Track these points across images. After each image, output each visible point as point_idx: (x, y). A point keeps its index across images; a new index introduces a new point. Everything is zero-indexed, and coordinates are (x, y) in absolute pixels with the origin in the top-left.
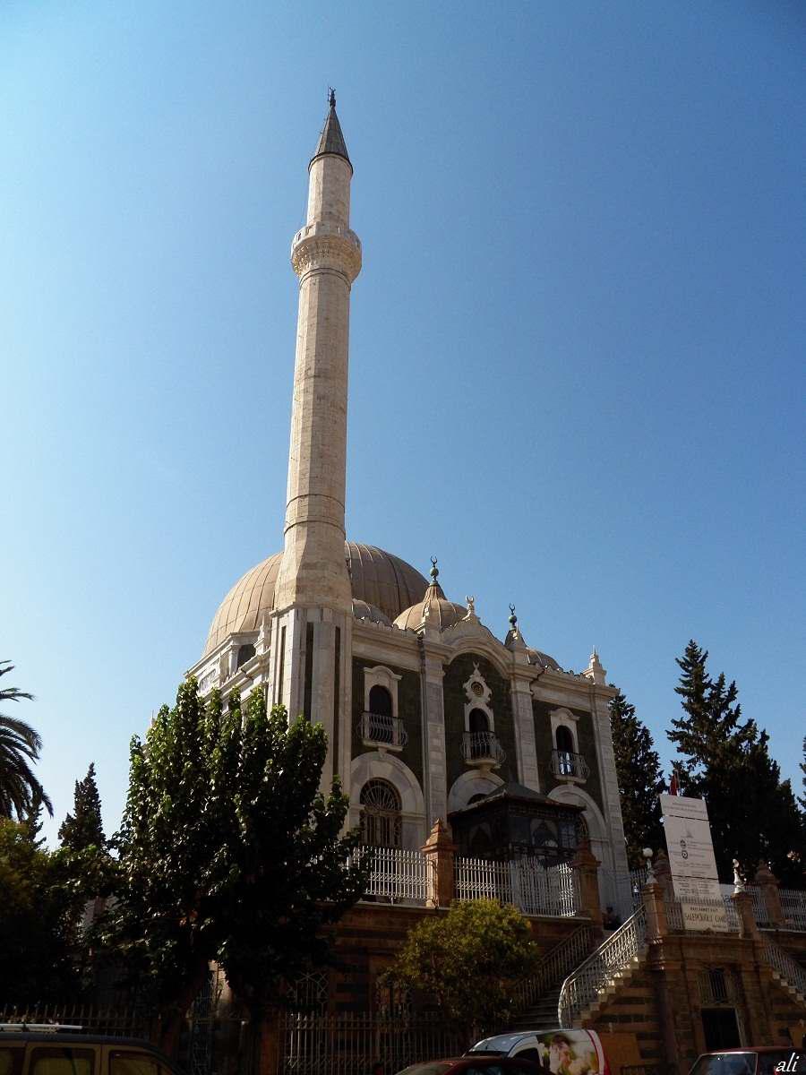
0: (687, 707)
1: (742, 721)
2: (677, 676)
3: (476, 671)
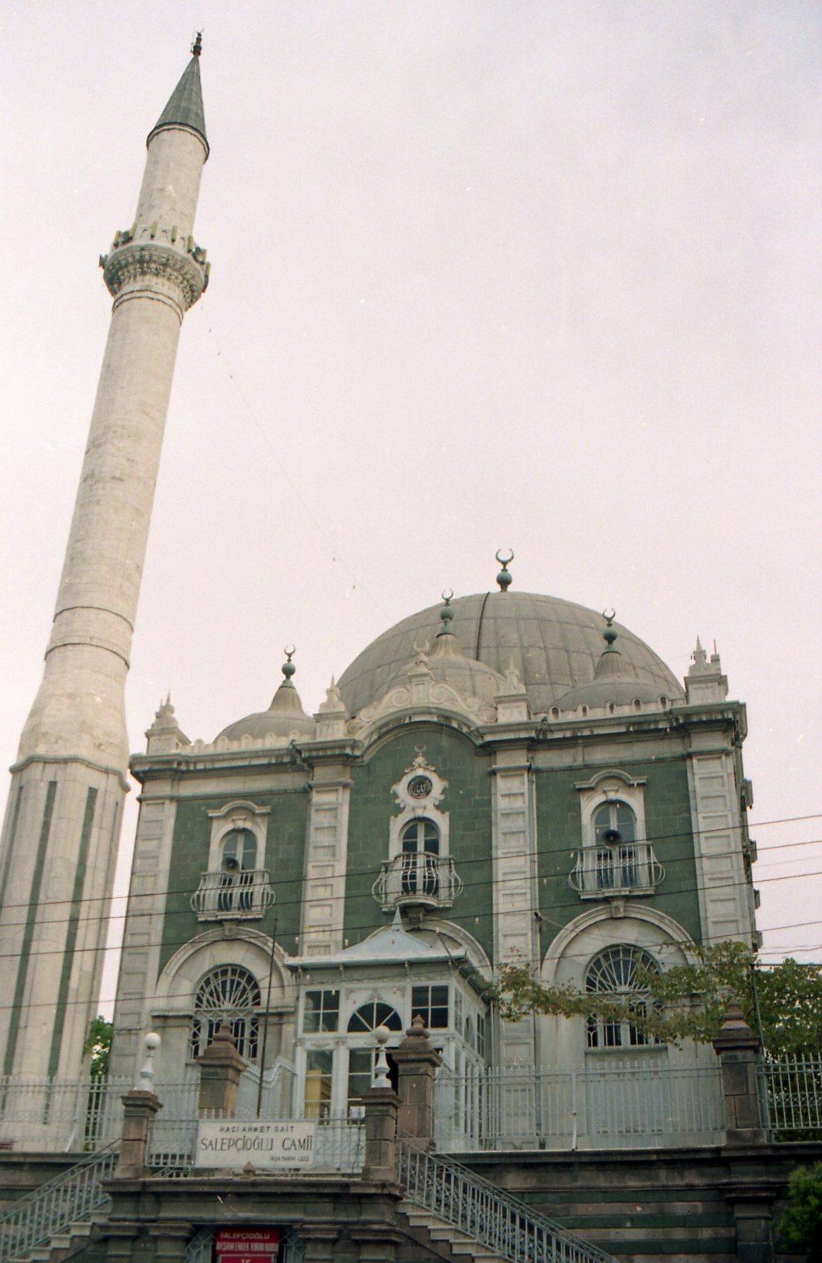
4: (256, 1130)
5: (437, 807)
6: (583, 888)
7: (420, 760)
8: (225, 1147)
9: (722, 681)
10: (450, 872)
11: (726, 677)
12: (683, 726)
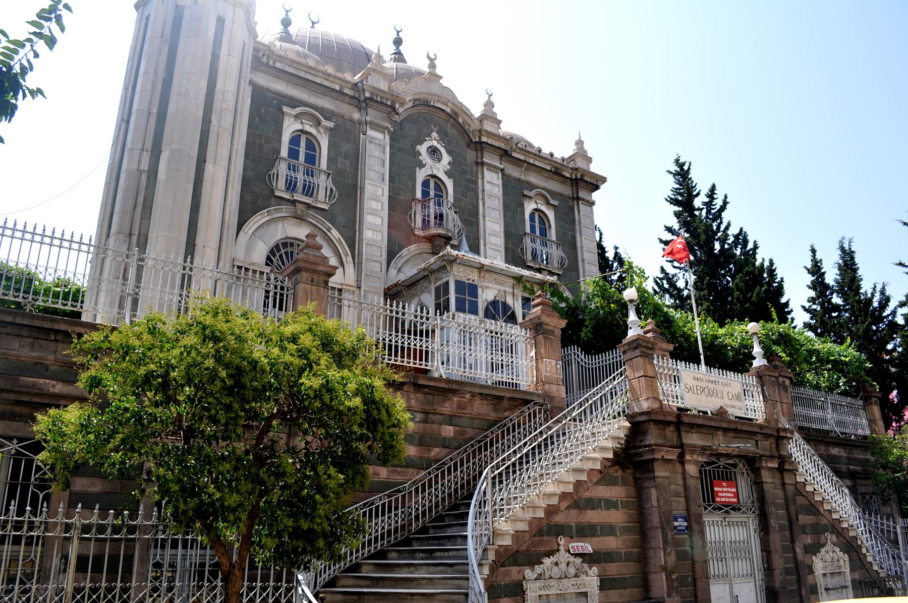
0: (677, 215)
1: (734, 231)
2: (670, 184)
3: (434, 134)
5: (446, 173)
12: (576, 179)
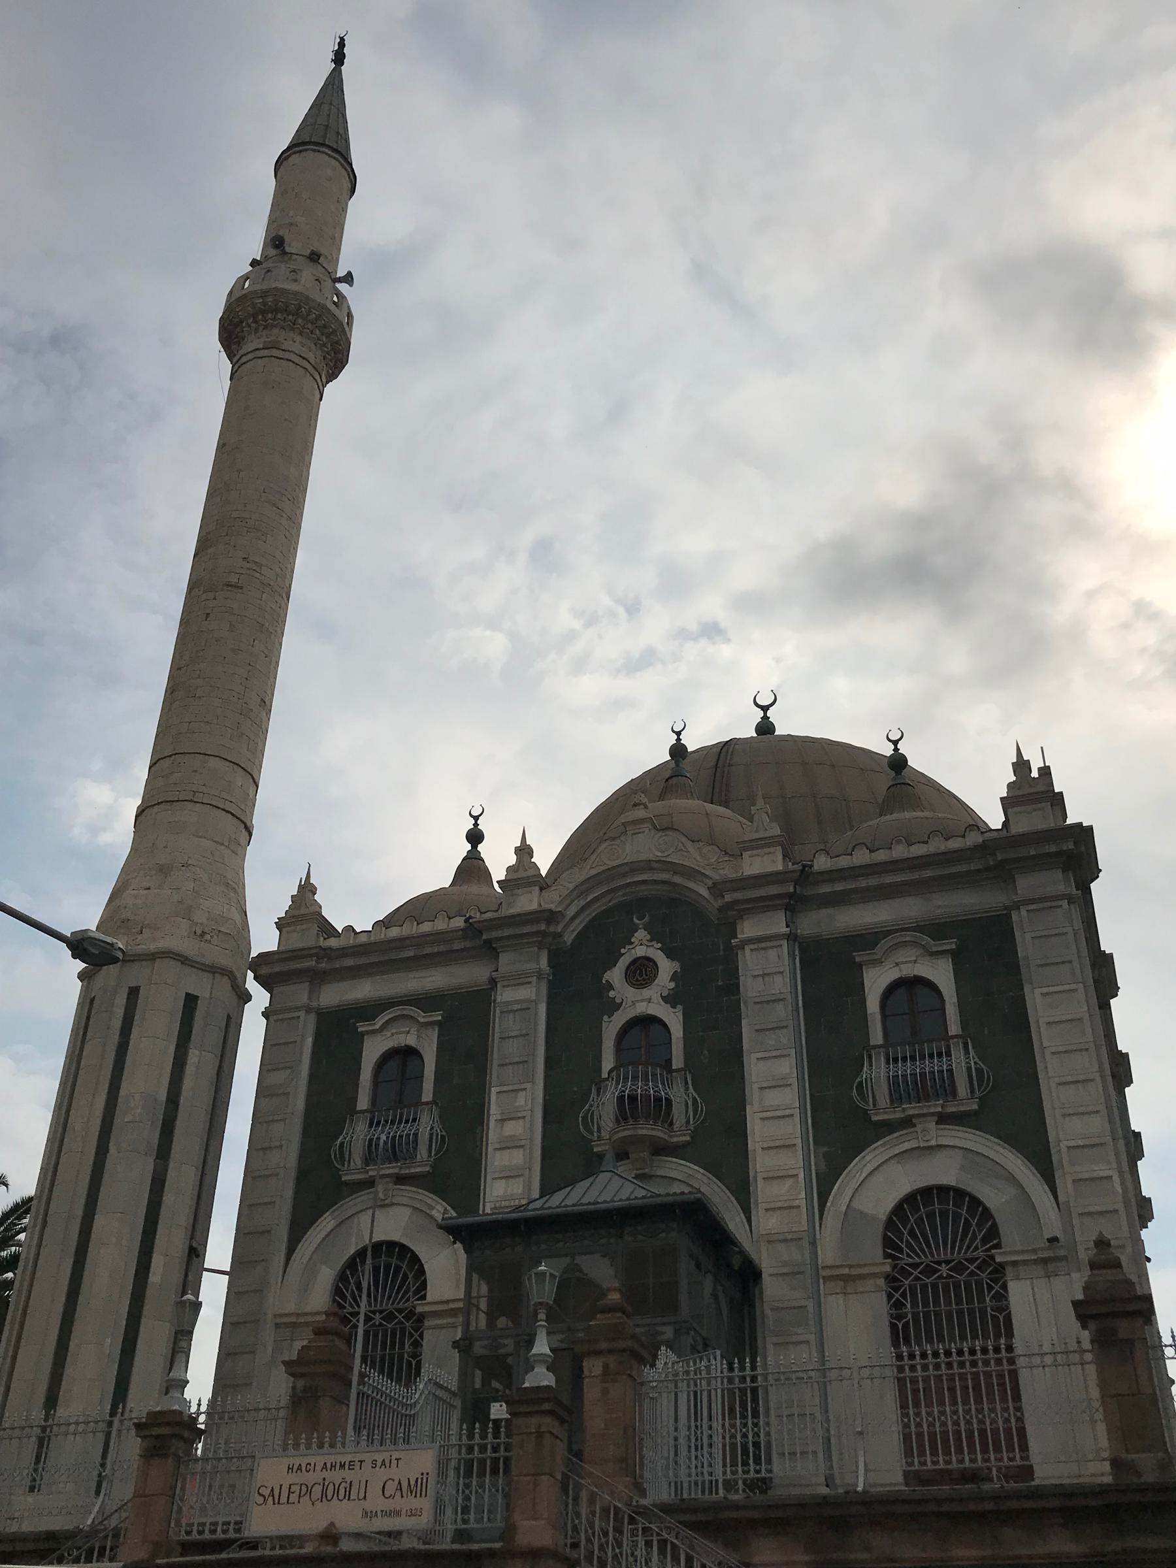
4: (342, 1466)
6: (874, 1105)
7: (641, 935)
8: (293, 1497)
9: (1058, 800)
10: (687, 1089)
11: (1029, 761)
